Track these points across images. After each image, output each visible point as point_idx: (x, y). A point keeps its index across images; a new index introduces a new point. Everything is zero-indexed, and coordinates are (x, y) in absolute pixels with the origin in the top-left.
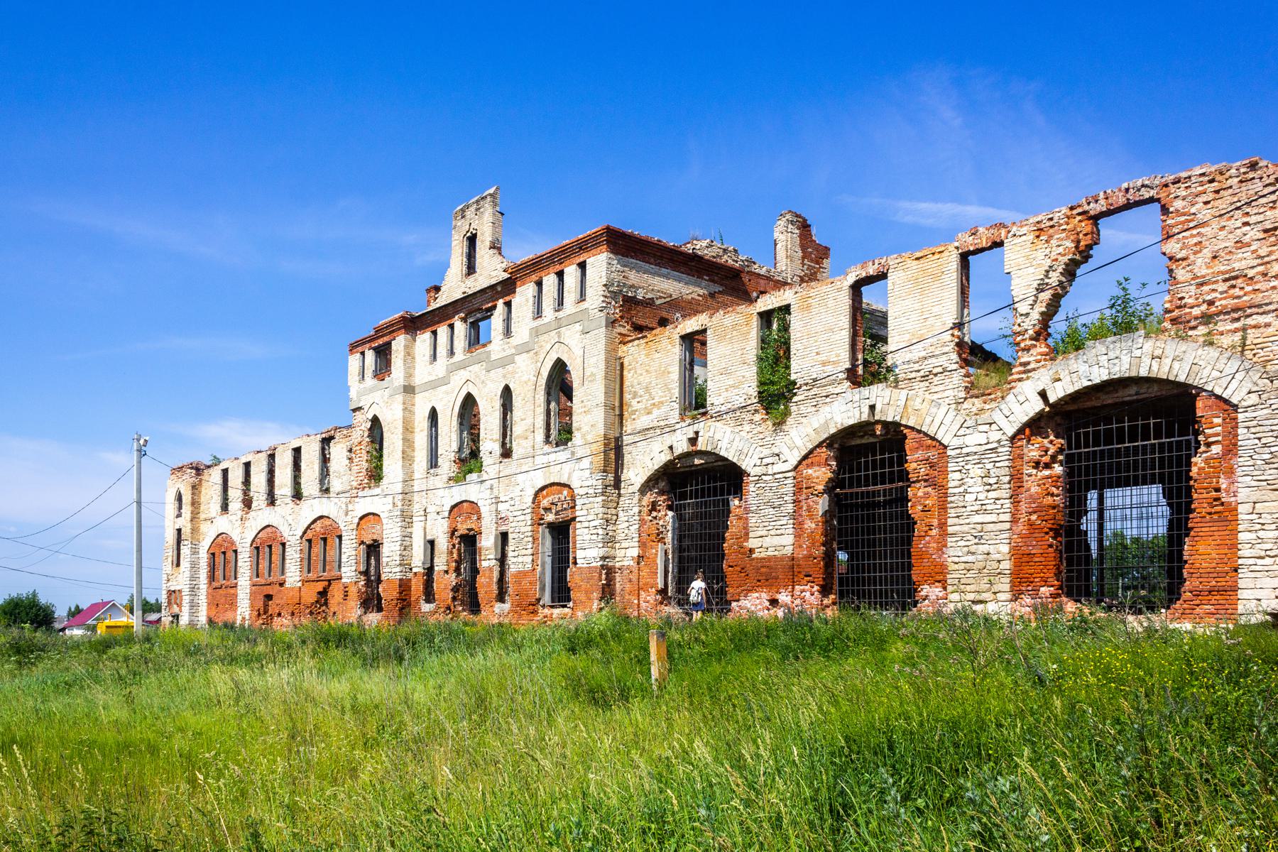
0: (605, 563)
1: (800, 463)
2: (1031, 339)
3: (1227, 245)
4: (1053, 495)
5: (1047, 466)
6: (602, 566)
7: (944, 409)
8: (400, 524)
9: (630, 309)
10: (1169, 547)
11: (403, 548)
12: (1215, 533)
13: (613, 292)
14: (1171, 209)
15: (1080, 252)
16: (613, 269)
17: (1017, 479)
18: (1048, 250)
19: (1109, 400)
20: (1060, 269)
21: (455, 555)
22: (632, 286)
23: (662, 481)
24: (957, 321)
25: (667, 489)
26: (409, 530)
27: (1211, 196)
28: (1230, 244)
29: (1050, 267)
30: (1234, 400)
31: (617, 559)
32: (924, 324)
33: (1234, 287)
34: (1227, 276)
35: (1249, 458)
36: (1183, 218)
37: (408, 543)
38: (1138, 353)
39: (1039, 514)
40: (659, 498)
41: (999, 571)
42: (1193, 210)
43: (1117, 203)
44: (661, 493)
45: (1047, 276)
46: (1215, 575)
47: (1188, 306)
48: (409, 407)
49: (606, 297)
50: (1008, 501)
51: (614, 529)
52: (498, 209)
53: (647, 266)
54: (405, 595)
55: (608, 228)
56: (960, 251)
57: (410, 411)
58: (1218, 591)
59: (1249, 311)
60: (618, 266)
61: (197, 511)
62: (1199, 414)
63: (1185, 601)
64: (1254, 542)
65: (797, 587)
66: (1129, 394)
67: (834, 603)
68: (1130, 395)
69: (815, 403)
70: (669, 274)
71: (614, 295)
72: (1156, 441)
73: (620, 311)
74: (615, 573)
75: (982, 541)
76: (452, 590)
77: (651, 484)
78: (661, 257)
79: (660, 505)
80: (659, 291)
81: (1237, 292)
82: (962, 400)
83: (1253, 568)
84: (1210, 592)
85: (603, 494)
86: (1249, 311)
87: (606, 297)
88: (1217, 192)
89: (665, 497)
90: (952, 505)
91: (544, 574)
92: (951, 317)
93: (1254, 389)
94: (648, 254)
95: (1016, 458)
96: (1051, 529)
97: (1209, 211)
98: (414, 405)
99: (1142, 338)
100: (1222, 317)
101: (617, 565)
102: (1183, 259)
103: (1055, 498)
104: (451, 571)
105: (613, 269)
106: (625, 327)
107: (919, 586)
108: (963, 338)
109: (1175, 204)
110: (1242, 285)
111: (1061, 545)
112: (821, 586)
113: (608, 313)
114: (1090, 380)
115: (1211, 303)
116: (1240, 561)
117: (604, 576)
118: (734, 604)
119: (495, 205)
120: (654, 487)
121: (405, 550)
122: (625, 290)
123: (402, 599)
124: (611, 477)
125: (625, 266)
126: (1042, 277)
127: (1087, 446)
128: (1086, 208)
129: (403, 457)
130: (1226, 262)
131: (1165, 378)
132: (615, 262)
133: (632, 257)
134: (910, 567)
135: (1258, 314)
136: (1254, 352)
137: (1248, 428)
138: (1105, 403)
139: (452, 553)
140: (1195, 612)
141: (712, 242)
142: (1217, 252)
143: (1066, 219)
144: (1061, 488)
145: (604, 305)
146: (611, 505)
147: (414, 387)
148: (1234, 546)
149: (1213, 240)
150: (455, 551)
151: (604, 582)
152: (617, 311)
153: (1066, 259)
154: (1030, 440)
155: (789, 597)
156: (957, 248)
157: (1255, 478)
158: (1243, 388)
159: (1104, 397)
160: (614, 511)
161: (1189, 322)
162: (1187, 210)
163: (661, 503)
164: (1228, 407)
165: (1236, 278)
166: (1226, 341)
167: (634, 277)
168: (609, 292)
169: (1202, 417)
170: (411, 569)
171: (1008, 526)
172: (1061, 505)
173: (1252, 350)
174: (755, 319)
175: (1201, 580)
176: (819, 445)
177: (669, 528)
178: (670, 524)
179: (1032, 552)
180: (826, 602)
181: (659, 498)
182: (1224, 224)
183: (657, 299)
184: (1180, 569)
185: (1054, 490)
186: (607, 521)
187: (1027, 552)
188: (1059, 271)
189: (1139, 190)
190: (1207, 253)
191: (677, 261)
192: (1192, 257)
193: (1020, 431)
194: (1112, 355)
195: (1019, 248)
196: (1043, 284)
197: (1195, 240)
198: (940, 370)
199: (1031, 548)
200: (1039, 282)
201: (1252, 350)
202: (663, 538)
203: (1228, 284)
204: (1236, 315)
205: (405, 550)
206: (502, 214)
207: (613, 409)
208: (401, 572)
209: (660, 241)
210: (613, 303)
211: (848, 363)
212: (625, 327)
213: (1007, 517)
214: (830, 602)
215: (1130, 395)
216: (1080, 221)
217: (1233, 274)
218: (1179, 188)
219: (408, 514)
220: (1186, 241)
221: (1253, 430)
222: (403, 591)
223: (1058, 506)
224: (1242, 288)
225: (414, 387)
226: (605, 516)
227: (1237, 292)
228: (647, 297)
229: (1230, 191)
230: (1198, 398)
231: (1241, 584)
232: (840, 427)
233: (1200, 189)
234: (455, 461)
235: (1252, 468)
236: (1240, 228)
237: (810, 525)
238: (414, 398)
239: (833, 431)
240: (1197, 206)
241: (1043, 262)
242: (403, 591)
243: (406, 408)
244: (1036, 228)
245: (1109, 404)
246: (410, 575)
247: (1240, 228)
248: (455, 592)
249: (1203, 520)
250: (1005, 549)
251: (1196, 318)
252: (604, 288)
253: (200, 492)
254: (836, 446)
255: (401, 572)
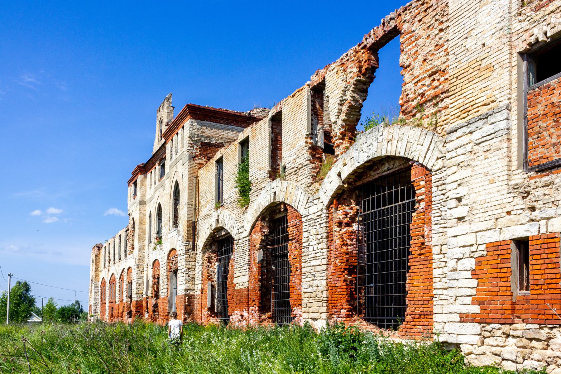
0: (187, 293)
1: (251, 230)
2: (340, 139)
3: (430, 49)
4: (347, 245)
5: (348, 225)
6: (186, 294)
7: (300, 191)
8: (136, 272)
9: (206, 150)
10: (406, 283)
11: (138, 285)
12: (422, 270)
13: (194, 140)
14: (403, 31)
15: (364, 75)
16: (194, 128)
17: (329, 236)
18: (345, 76)
19: (374, 175)
20: (351, 89)
21: (155, 288)
22: (208, 137)
23: (215, 245)
24: (308, 133)
25: (217, 249)
26: (142, 275)
27: (422, 14)
28: (432, 48)
29: (346, 88)
30: (429, 167)
31: (195, 291)
32: (295, 137)
33: (434, 80)
34: (430, 72)
35: (438, 211)
36: (408, 36)
37: (141, 282)
38: (380, 139)
39: (341, 258)
40: (212, 255)
41: (322, 298)
42: (413, 29)
43: (379, 35)
44: (213, 252)
45: (345, 95)
46: (422, 302)
47: (410, 100)
48: (143, 212)
49: (190, 143)
50: (325, 250)
51: (193, 273)
52: (171, 105)
53: (218, 125)
54: (139, 309)
55: (188, 105)
56: (311, 87)
57: (143, 214)
58: (424, 315)
59: (442, 96)
60: (198, 126)
61: (97, 267)
62: (412, 180)
63: (407, 322)
64: (441, 276)
65: (250, 307)
66: (385, 170)
67: (269, 318)
68: (385, 171)
69: (257, 194)
70: (234, 128)
71: (195, 142)
72: (401, 203)
73: (199, 151)
74: (194, 298)
75: (315, 278)
76: (153, 306)
77: (207, 247)
78: (228, 120)
79: (213, 259)
80: (226, 138)
81: (436, 83)
82: (310, 184)
83: (442, 297)
84: (420, 315)
85: (186, 254)
86: (442, 96)
87: (190, 143)
88: (425, 11)
89: (215, 255)
90: (304, 254)
91: (172, 299)
92: (305, 131)
93: (440, 156)
94: (219, 118)
95: (329, 219)
96: (345, 269)
97: (421, 26)
98: (145, 211)
99: (382, 127)
100: (428, 104)
101: (196, 293)
102: (409, 66)
103: (349, 247)
104: (153, 297)
105: (194, 128)
106: (203, 160)
107: (293, 307)
108: (316, 144)
109: (404, 26)
110: (438, 78)
111: (356, 280)
112: (259, 307)
113: (192, 153)
114: (359, 162)
115: (423, 95)
116: (435, 292)
117: (187, 300)
118: (231, 317)
119: (169, 102)
120: (210, 249)
121: (139, 285)
122: (203, 139)
123: (137, 311)
124: (191, 244)
125: (203, 126)
126: (341, 95)
127: (368, 210)
128: (365, 43)
129: (139, 238)
130: (430, 62)
131: (394, 155)
132: (196, 124)
133: (207, 121)
134: (288, 295)
135: (447, 97)
136: (442, 127)
137: (437, 186)
138: (374, 178)
139: (154, 287)
140: (413, 331)
141: (265, 109)
142: (426, 56)
143: (354, 53)
144: (354, 240)
145: (189, 148)
146: (191, 260)
147: (146, 202)
148: (430, 280)
149: (424, 47)
150: (155, 286)
151: (187, 304)
152: (198, 151)
153: (353, 81)
154: (338, 208)
155: (247, 314)
156: (309, 85)
157: (442, 226)
158: (434, 156)
159: (373, 174)
160: (193, 263)
161: (411, 111)
162: (410, 29)
163: (213, 258)
164: (427, 171)
165: (435, 73)
166: (426, 122)
167: (208, 132)
168: (192, 141)
169: (414, 181)
170: (143, 296)
171: (325, 267)
172: (355, 252)
173: (441, 126)
174: (238, 145)
175: (415, 306)
176: (257, 220)
177: (216, 272)
178: (216, 270)
179: (337, 285)
180: (263, 317)
181: (212, 255)
182: (429, 33)
183: (225, 143)
184: (404, 297)
185: (349, 242)
186: (189, 269)
187: (334, 285)
188: (351, 89)
189: (389, 23)
190: (420, 58)
191: (239, 121)
192: (413, 64)
193: (331, 202)
194: (369, 143)
195: (331, 79)
196: (343, 100)
197: (414, 50)
198: (300, 166)
199: (336, 282)
200: (340, 99)
201: (441, 126)
202: (212, 278)
203: (431, 78)
204: (434, 101)
205: (139, 285)
206: (174, 107)
207: (192, 206)
208: (137, 297)
209: (227, 111)
210: (195, 147)
211: (268, 167)
212: (203, 160)
213: (325, 261)
214: (267, 317)
215: (385, 171)
216: (363, 53)
217: (433, 70)
218: (406, 14)
219: (141, 267)
220: (409, 52)
221: (440, 188)
222: (138, 307)
223: (352, 252)
224: (439, 80)
225: (146, 202)
226: (187, 266)
227: (436, 83)
228: (218, 142)
229: (433, 8)
230: (412, 168)
231: (436, 309)
232: (264, 208)
233: (417, 11)
234: (156, 239)
235: (439, 218)
236: (438, 34)
237: (254, 269)
238: (146, 207)
239: (261, 210)
240: (415, 25)
241: (342, 85)
242: (138, 307)
243: (141, 213)
244: (341, 63)
245: (376, 179)
246: (142, 299)
247: (438, 34)
248: (155, 308)
249: (416, 260)
250: (324, 283)
251: (414, 108)
252: (189, 139)
253: (99, 258)
254: (267, 219)
255: (137, 297)
